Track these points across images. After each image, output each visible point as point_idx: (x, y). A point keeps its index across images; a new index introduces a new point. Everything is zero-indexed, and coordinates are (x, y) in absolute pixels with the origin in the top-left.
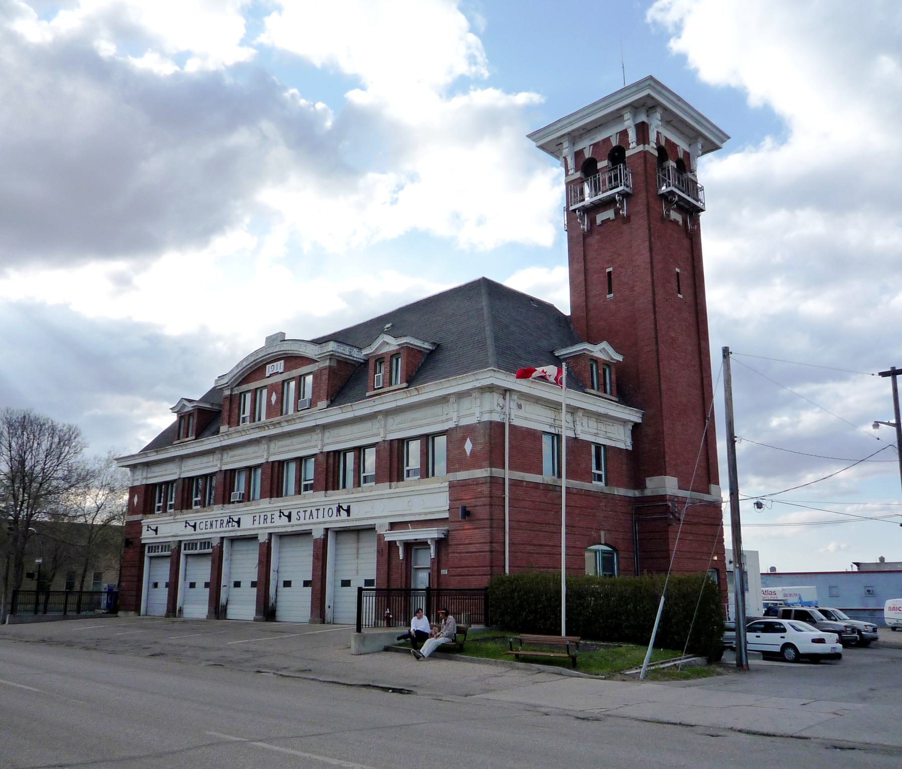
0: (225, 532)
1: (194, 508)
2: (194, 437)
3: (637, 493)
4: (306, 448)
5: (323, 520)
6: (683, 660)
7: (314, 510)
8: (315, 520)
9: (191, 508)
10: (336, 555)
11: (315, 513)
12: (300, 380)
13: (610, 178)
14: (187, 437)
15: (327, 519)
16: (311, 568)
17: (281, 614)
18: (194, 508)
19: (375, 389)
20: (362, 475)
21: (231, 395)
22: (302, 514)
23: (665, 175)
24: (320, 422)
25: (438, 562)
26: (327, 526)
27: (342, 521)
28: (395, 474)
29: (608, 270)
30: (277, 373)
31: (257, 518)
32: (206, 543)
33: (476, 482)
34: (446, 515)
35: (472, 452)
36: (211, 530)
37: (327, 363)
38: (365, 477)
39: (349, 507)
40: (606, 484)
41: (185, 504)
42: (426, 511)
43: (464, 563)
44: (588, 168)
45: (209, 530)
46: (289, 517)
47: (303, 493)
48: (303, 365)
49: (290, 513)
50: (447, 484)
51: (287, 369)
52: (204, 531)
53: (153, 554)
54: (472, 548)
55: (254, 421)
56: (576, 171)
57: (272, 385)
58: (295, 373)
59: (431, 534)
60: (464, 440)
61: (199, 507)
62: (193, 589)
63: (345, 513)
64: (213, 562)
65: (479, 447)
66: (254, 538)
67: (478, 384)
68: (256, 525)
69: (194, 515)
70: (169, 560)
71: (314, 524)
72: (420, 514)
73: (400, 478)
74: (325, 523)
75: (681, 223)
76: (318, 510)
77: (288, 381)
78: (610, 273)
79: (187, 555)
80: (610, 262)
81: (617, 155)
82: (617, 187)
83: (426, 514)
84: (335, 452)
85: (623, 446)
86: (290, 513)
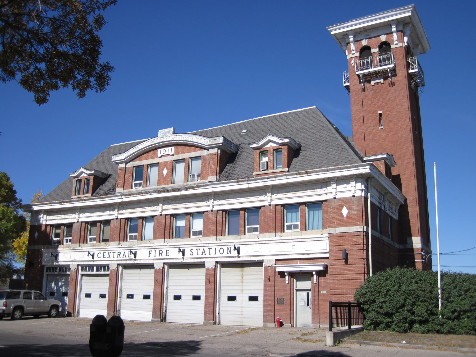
1: (89, 243)
2: (91, 195)
5: (215, 256)
7: (214, 249)
8: (208, 255)
10: (47, 284)
11: (207, 251)
13: (380, 60)
14: (83, 194)
15: (218, 255)
17: (169, 319)
20: (192, 230)
22: (195, 251)
23: (413, 62)
27: (233, 257)
28: (278, 226)
29: (379, 112)
31: (153, 252)
32: (106, 267)
33: (352, 234)
34: (327, 255)
36: (109, 259)
38: (193, 232)
39: (136, 252)
41: (83, 240)
43: (342, 286)
45: (106, 259)
46: (93, 256)
47: (192, 237)
49: (94, 254)
50: (327, 235)
51: (176, 153)
52: (102, 259)
53: (84, 272)
54: (350, 277)
55: (79, 194)
57: (163, 163)
60: (342, 208)
61: (95, 242)
62: (88, 299)
63: (92, 257)
64: (111, 280)
65: (354, 213)
66: (150, 266)
68: (152, 256)
70: (108, 278)
73: (282, 230)
74: (217, 257)
77: (177, 161)
78: (380, 114)
79: (83, 275)
80: (380, 108)
81: (385, 47)
82: (389, 64)
85: (395, 218)
86: (94, 254)
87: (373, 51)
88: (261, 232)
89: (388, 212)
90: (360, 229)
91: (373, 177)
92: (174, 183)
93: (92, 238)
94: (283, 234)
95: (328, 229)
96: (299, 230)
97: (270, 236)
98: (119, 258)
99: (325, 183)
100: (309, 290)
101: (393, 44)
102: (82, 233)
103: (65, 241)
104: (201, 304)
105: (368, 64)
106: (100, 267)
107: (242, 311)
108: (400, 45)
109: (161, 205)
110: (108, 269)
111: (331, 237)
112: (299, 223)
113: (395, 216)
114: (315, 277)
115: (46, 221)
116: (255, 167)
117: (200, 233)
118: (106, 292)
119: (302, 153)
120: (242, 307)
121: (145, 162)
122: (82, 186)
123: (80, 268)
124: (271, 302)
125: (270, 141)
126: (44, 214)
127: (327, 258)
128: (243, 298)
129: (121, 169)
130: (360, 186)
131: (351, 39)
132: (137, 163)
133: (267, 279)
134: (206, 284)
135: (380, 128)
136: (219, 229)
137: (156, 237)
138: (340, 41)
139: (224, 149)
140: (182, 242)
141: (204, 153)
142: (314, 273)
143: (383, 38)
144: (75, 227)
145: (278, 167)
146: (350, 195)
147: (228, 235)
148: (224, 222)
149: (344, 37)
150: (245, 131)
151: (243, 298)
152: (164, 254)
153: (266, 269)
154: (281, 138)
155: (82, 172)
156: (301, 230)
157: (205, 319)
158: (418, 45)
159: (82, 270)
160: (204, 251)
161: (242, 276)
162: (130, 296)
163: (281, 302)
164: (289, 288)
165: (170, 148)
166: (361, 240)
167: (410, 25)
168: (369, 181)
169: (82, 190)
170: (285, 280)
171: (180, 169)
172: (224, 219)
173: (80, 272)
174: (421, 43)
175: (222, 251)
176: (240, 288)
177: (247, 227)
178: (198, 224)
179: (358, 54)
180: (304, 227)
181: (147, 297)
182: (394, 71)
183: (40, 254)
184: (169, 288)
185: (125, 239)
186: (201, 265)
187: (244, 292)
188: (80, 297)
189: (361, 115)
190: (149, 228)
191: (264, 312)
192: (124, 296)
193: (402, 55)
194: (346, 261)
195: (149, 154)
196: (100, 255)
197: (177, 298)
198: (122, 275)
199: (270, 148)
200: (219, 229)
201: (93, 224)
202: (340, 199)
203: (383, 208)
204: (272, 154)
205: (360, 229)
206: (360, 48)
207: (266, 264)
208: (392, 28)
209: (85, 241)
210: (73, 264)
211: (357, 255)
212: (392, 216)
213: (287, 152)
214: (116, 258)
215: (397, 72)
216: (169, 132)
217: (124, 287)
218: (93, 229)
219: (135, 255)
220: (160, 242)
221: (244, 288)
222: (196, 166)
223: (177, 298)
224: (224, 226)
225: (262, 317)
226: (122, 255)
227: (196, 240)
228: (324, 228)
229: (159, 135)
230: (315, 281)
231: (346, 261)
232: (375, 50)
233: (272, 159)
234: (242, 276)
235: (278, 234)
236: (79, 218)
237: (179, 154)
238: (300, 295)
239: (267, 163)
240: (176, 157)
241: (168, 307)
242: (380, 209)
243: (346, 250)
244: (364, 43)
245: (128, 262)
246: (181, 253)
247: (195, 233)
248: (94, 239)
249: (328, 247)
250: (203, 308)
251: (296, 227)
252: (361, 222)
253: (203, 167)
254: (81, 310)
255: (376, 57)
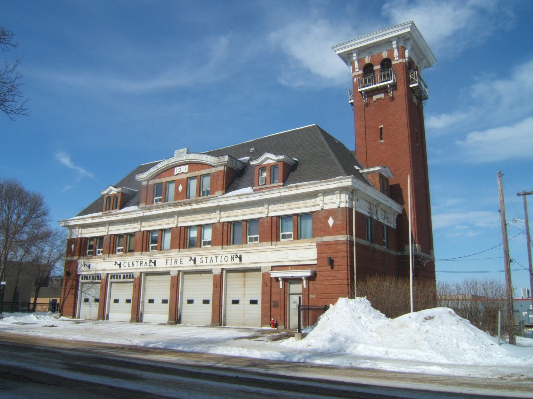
0: (143, 269)
1: (117, 253)
3: (400, 254)
4: (207, 219)
5: (221, 263)
6: (151, 346)
7: (218, 258)
8: (215, 263)
9: (115, 253)
11: (214, 259)
12: (200, 179)
15: (223, 262)
16: (212, 293)
18: (117, 253)
19: (259, 185)
20: (203, 241)
21: (148, 185)
22: (204, 260)
24: (221, 204)
25: (307, 292)
26: (224, 267)
27: (236, 264)
28: (274, 236)
29: (380, 127)
30: (183, 173)
31: (169, 261)
33: (337, 243)
34: (315, 262)
35: (334, 225)
36: (133, 267)
37: (222, 168)
38: (204, 242)
39: (155, 261)
40: (387, 248)
41: (112, 251)
42: (300, 259)
44: (368, 69)
45: (131, 267)
46: (120, 265)
47: (203, 247)
48: (203, 169)
49: (120, 263)
50: (315, 244)
52: (127, 267)
54: (335, 282)
56: (360, 70)
57: (179, 180)
58: (197, 173)
59: (308, 273)
60: (328, 218)
61: (122, 253)
62: (151, 304)
64: (135, 287)
65: (339, 222)
66: (167, 273)
67: (341, 185)
69: (118, 258)
70: (132, 284)
71: (214, 265)
72: (295, 261)
73: (278, 239)
74: (222, 265)
75: (417, 104)
76: (217, 257)
78: (381, 129)
79: (112, 283)
80: (382, 122)
81: (386, 63)
82: (389, 80)
83: (300, 261)
84: (228, 222)
85: (392, 226)
86: (120, 263)
87: (375, 68)
88: (260, 241)
89: (381, 221)
90: (342, 238)
91: (358, 189)
92: (189, 198)
93: (286, 235)
94: (279, 243)
95: (316, 238)
96: (292, 239)
97: (267, 245)
98: (141, 267)
99: (314, 195)
100: (300, 294)
101: (394, 60)
102: (112, 245)
103: (97, 252)
104: (209, 307)
105: (369, 81)
106: (126, 276)
107: (244, 314)
108: (401, 60)
109: (218, 212)
110: (133, 278)
111: (319, 245)
112: (292, 233)
113: (393, 225)
114: (305, 282)
115: (81, 234)
116: (255, 183)
117: (209, 243)
118: (168, 297)
119: (299, 168)
120: (244, 310)
121: (164, 180)
122: (112, 203)
123: (110, 276)
124: (268, 305)
125: (268, 158)
126: (79, 228)
127: (316, 264)
128: (245, 302)
129: (144, 186)
130: (344, 197)
131: (355, 58)
132: (157, 181)
133: (264, 283)
134: (213, 289)
135: (380, 141)
136: (225, 239)
137: (172, 247)
138: (346, 59)
139: (230, 166)
140: (194, 252)
141: (213, 170)
142: (303, 278)
143: (385, 55)
144: (106, 240)
145: (275, 181)
146: (335, 206)
147: (233, 244)
148: (229, 233)
149: (349, 56)
150: (253, 149)
151: (245, 302)
152: (179, 262)
153: (264, 275)
154: (277, 154)
155: (111, 190)
156: (294, 239)
157: (212, 321)
158: (422, 59)
159: (111, 278)
160: (212, 259)
161: (244, 282)
162: (151, 301)
163: (276, 305)
164: (282, 293)
165: (184, 167)
166: (344, 247)
167: (411, 41)
168: (354, 193)
169: (111, 206)
170: (279, 285)
171: (194, 184)
172: (229, 230)
173: (110, 280)
174: (425, 57)
175: (226, 258)
176: (242, 292)
177: (249, 237)
178: (208, 235)
179: (361, 72)
180: (297, 236)
181: (206, 302)
182: (394, 86)
183: (76, 263)
184: (184, 293)
185: (147, 250)
186: (210, 272)
187: (246, 296)
188: (182, 303)
189: (364, 129)
190: (168, 237)
191: (262, 315)
192: (147, 301)
193: (401, 72)
194: (332, 268)
195: (167, 172)
196: (126, 264)
197: (190, 302)
198: (144, 282)
199: (267, 164)
200: (225, 239)
201: (121, 236)
202: (327, 210)
203: (375, 217)
204: (269, 170)
205: (342, 238)
206: (363, 66)
207: (263, 271)
208: (392, 45)
209: (114, 252)
210: (103, 273)
211: (341, 262)
212: (389, 224)
213: (282, 168)
214: (139, 267)
215: (398, 87)
216: (184, 152)
217: (147, 293)
218: (121, 240)
219: (155, 263)
220: (175, 253)
221: (246, 292)
222: (207, 181)
223: (190, 302)
224: (229, 236)
225: (260, 319)
226: (144, 264)
227: (205, 249)
228: (314, 236)
229: (175, 155)
230: (305, 286)
231: (332, 268)
232: (377, 67)
233: (269, 174)
234: (244, 282)
235: (274, 243)
236: (220, 218)
237: (192, 171)
238: (293, 299)
239: (266, 178)
240: (189, 175)
241: (183, 311)
242: (371, 219)
243: (330, 258)
244: (367, 60)
245: (149, 270)
246: (192, 262)
247: (205, 243)
248: (122, 250)
249: (316, 254)
250: (211, 311)
251: (289, 236)
252: (345, 231)
253: (212, 183)
254: (110, 314)
255: (378, 75)
